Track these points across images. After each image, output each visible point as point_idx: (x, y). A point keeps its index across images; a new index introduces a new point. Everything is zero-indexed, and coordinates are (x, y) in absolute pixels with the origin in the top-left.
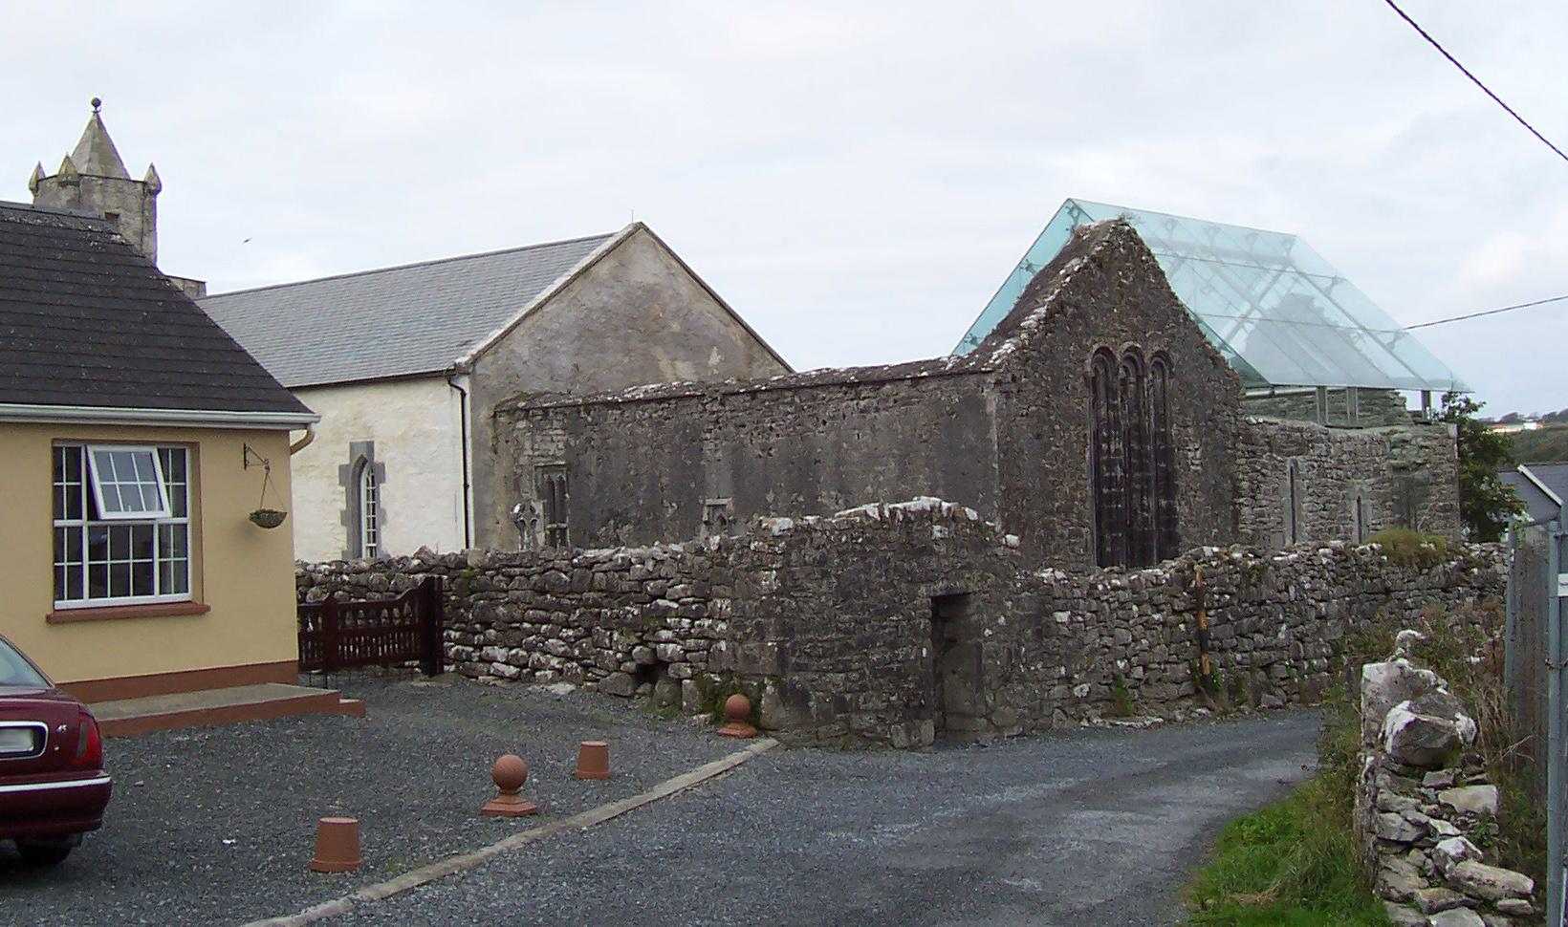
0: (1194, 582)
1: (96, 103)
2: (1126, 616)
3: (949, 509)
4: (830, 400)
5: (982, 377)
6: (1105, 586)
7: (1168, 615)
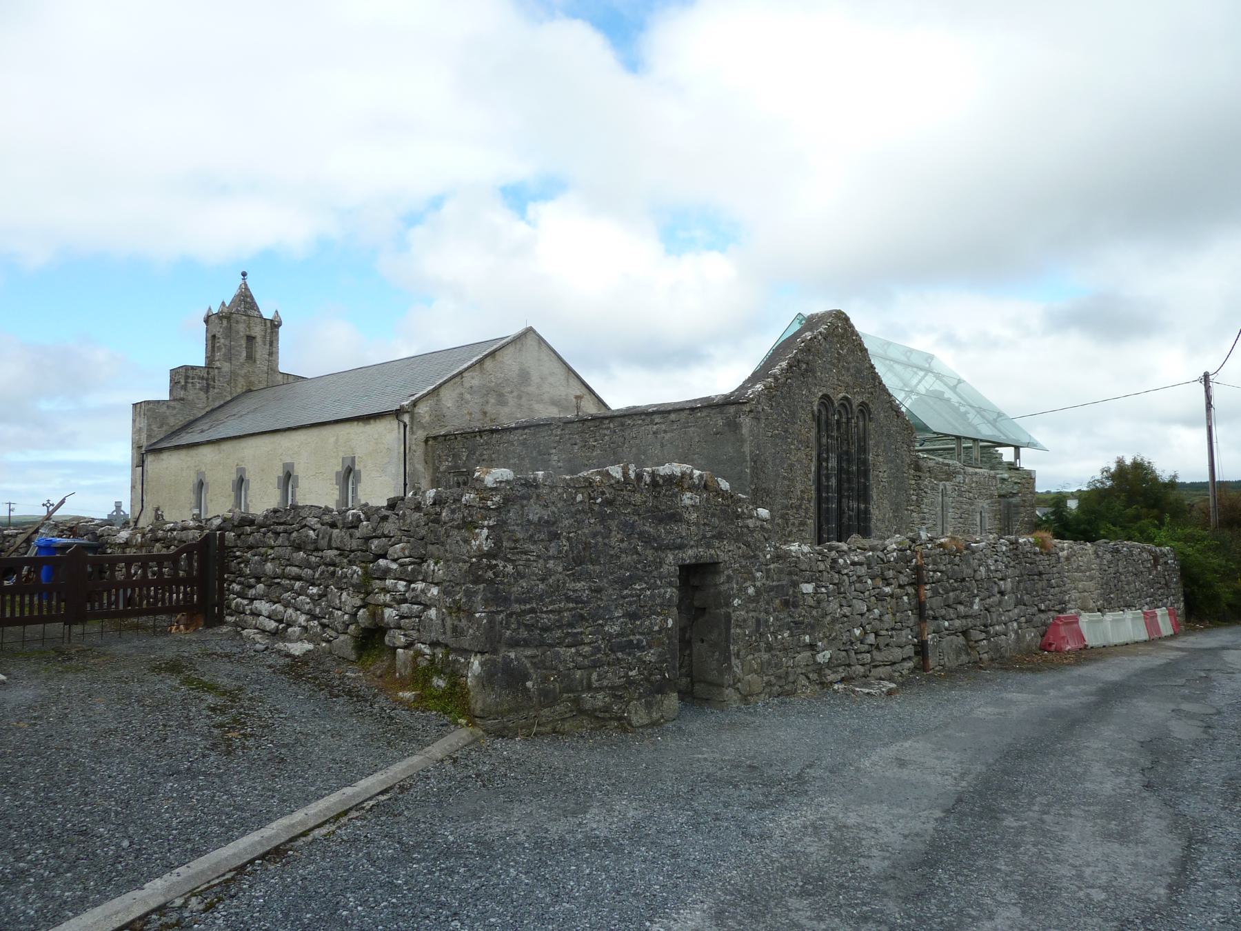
0: (914, 560)
1: (244, 274)
3: (701, 476)
4: (634, 425)
5: (740, 406)
6: (845, 561)
7: (895, 588)
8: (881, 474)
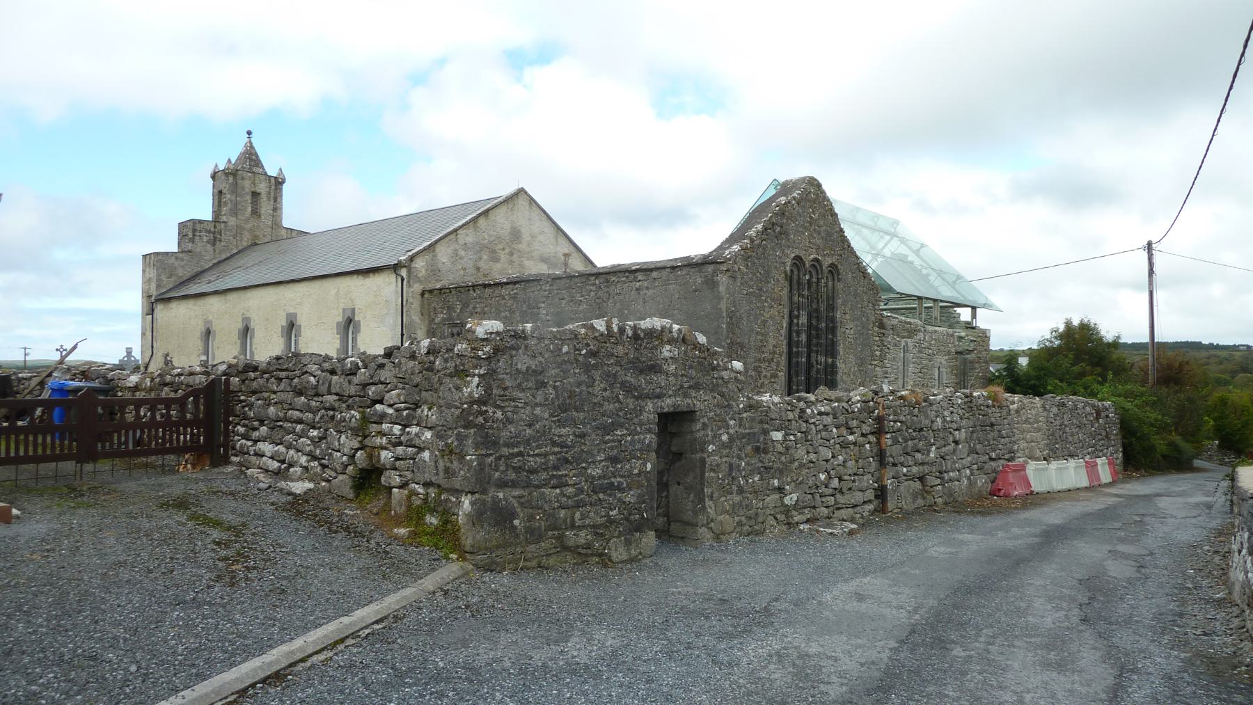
0: (876, 411)
1: (249, 133)
2: (828, 436)
3: (680, 330)
5: (718, 265)
8: (847, 331)
